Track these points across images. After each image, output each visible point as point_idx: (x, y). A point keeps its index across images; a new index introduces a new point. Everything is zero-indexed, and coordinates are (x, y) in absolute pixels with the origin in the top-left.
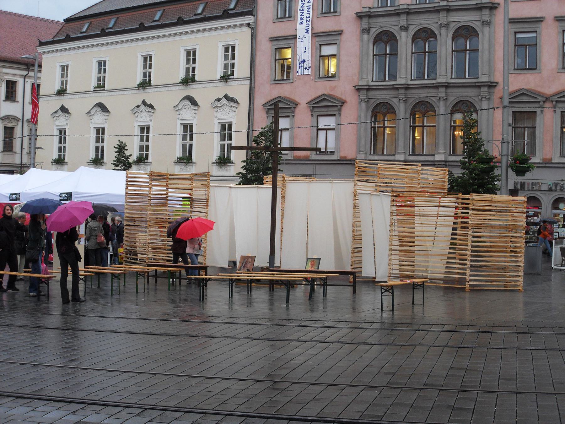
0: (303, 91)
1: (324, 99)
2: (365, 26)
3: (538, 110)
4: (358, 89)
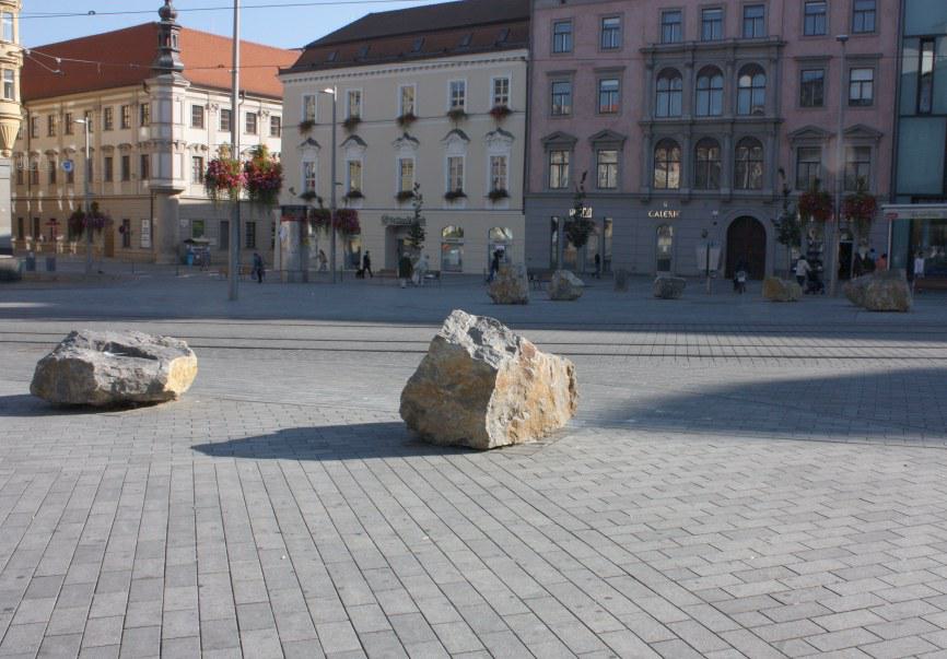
0: (584, 128)
1: (606, 135)
2: (649, 62)
3: (824, 146)
4: (641, 124)
